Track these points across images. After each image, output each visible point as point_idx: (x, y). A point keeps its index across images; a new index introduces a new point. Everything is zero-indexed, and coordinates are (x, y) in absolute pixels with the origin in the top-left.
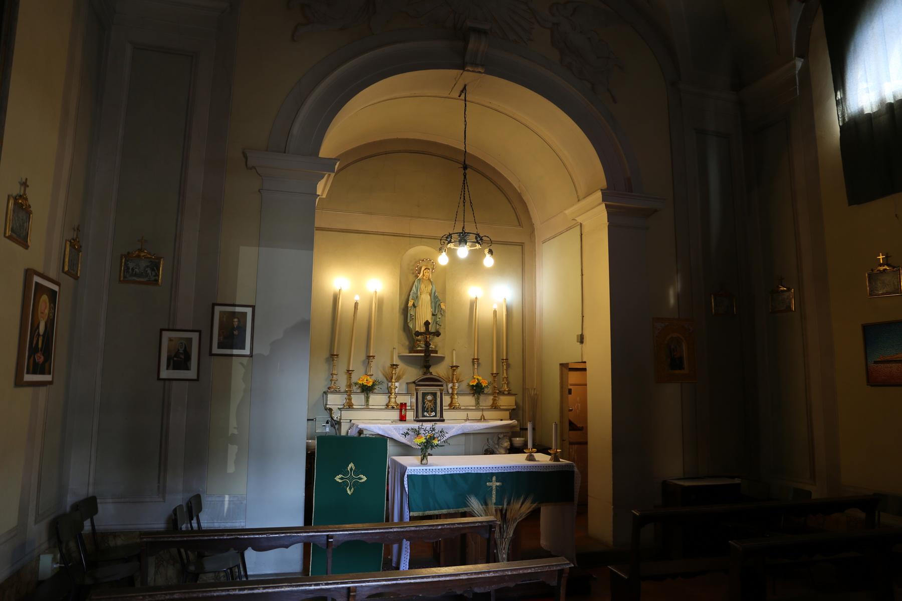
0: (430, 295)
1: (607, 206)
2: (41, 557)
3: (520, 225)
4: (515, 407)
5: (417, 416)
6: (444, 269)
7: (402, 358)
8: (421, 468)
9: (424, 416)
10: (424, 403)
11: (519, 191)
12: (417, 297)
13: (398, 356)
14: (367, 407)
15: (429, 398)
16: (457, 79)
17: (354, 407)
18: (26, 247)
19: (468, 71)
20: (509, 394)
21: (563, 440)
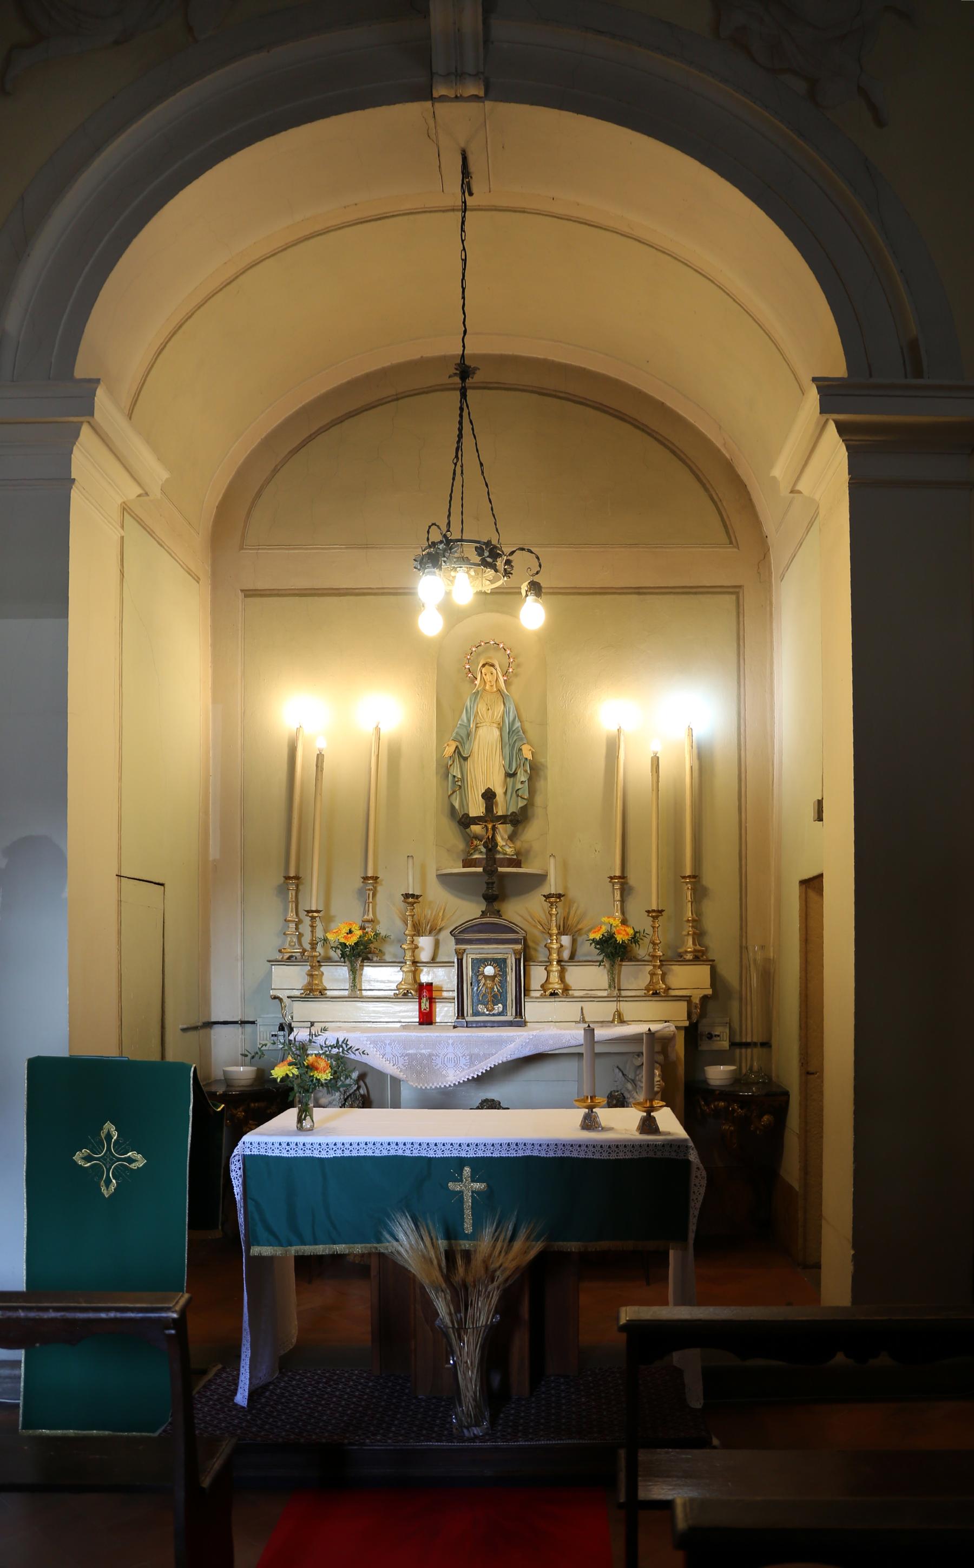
0: (501, 730)
1: (842, 429)
3: (731, 540)
4: (709, 992)
5: (461, 1013)
7: (446, 879)
8: (301, 1139)
9: (477, 1013)
11: (727, 456)
12: (468, 735)
13: (438, 876)
14: (355, 993)
16: (434, 137)
17: (329, 993)
19: (443, 99)
20: (699, 958)
21: (808, 1073)
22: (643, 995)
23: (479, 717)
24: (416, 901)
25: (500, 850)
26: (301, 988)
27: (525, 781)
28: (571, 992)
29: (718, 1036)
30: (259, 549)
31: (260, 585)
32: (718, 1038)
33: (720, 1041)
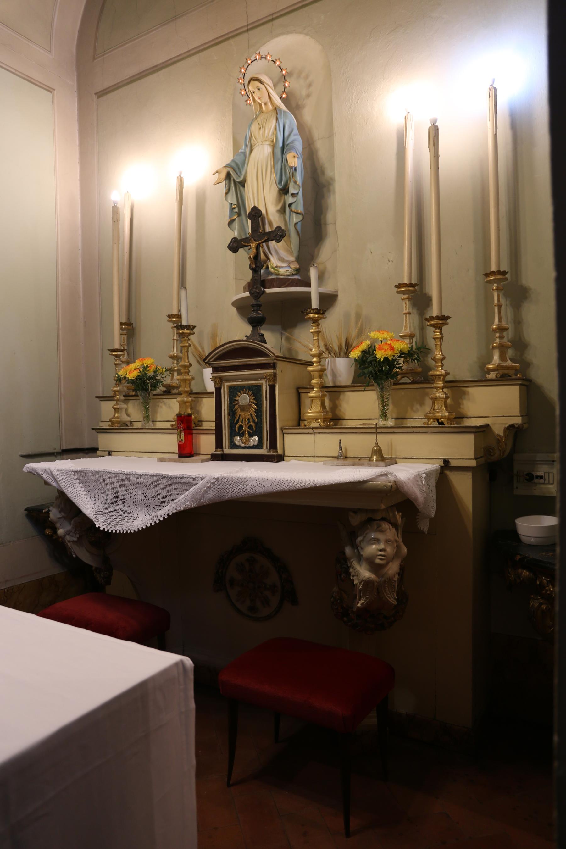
2: (349, 383)
5: (219, 444)
6: (381, 369)
9: (233, 446)
10: (232, 412)
15: (244, 399)
18: (196, 326)
22: (170, 427)
23: (254, 140)
24: (192, 332)
25: (272, 270)
26: (109, 421)
27: (298, 194)
28: (344, 422)
29: (541, 477)
30: (104, 55)
31: (108, 84)
32: (542, 481)
33: (544, 483)
